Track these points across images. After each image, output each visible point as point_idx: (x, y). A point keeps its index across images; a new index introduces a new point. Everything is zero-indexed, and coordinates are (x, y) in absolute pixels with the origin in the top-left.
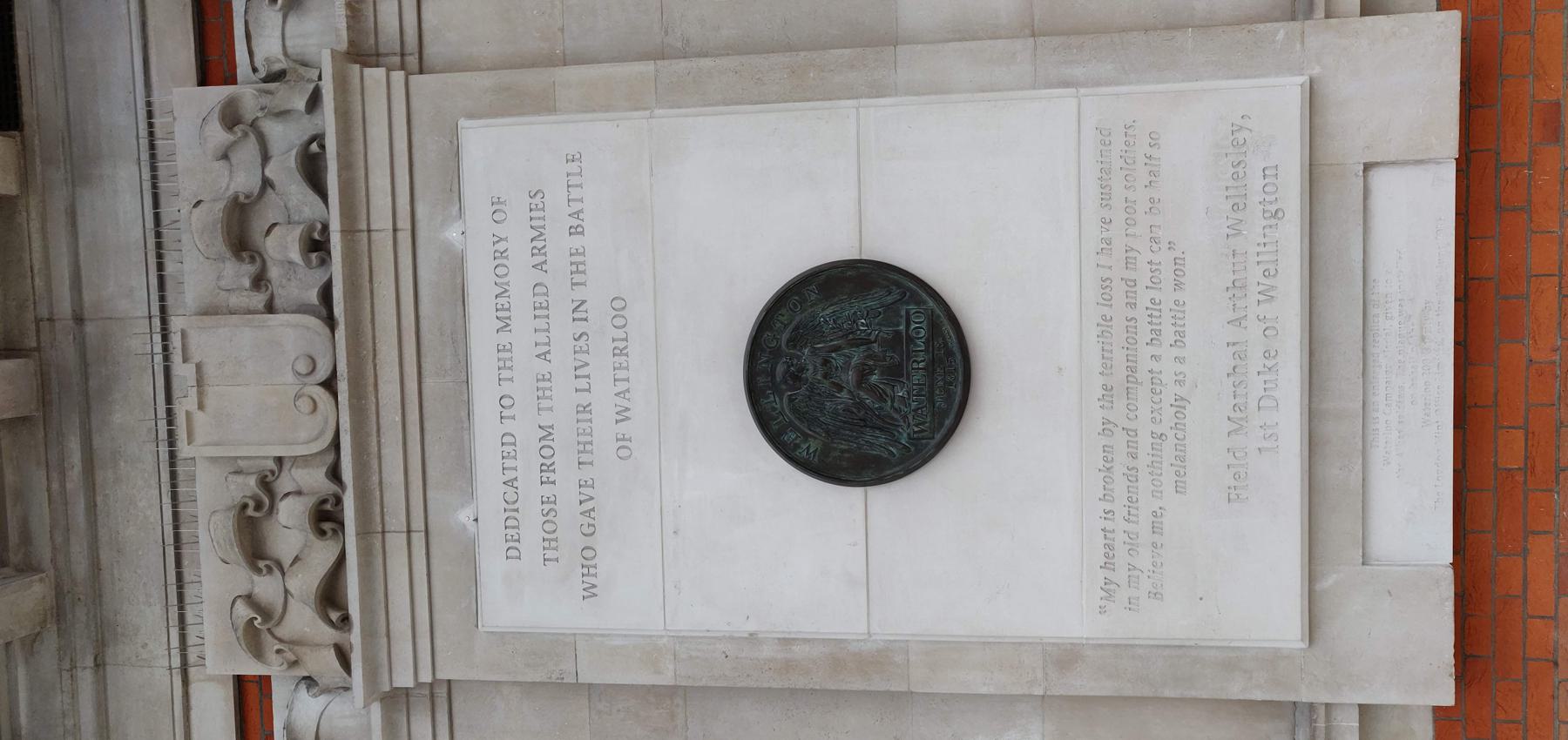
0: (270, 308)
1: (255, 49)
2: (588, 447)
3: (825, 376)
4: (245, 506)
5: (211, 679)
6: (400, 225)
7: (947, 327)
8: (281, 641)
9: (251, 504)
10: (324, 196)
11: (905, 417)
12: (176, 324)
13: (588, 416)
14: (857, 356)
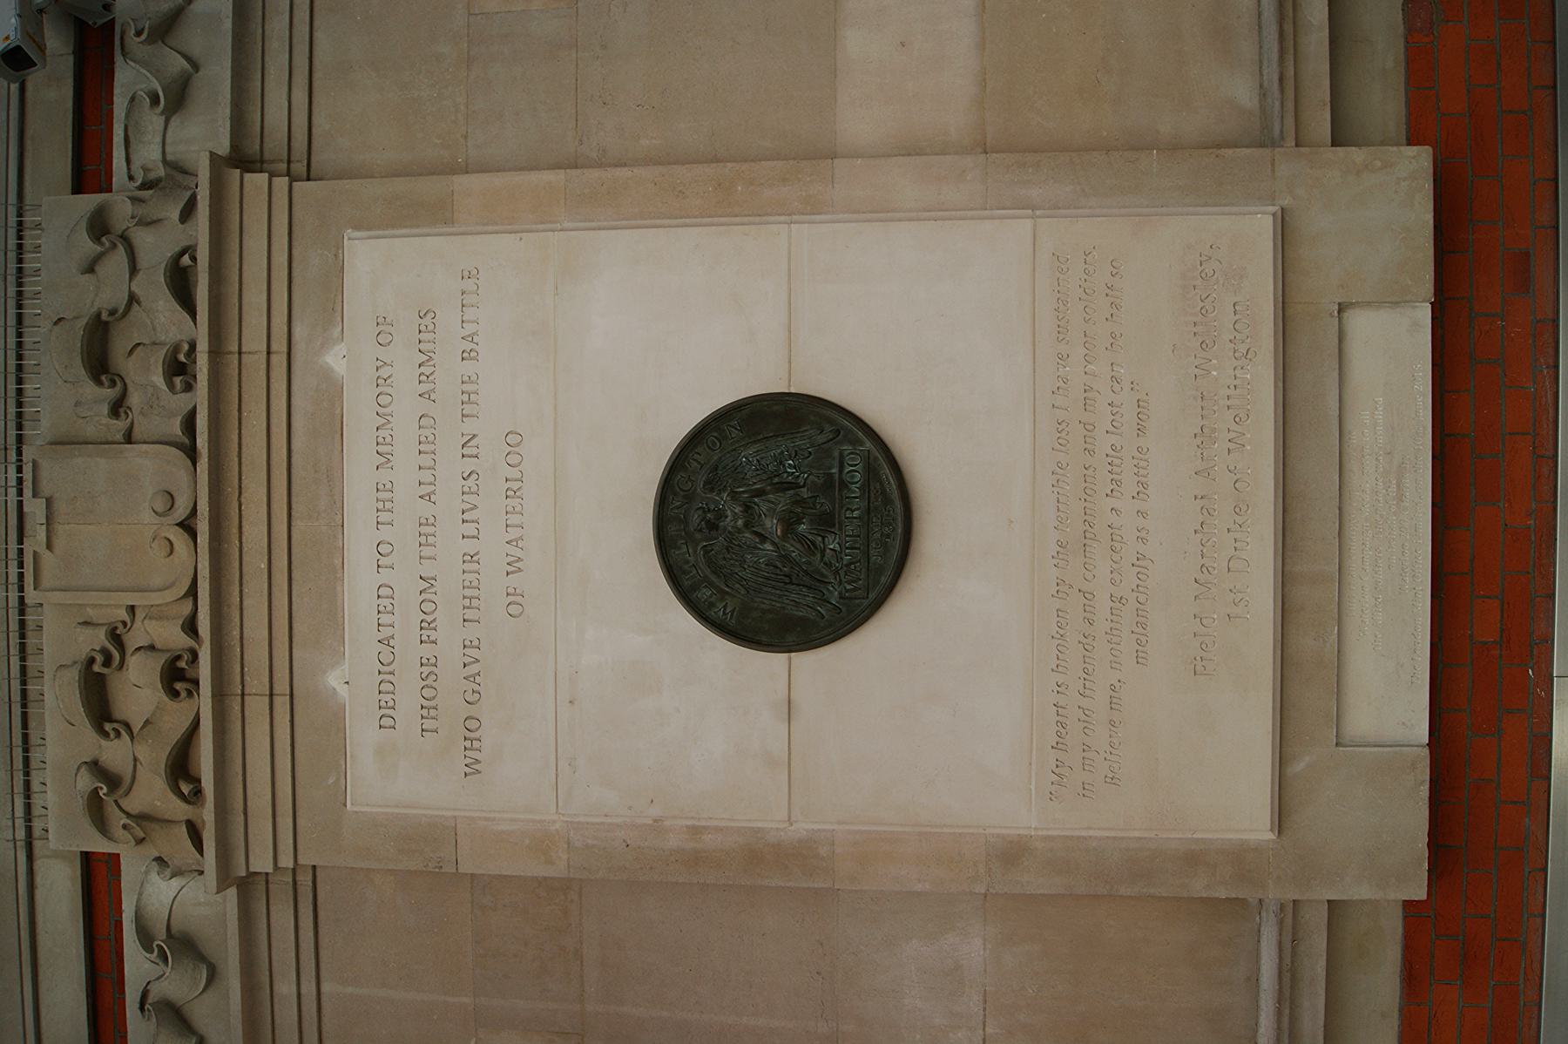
0: (129, 438)
1: (134, 157)
2: (475, 603)
3: (746, 525)
4: (92, 661)
5: (57, 855)
6: (274, 347)
7: (886, 471)
8: (128, 815)
9: (99, 658)
10: (192, 312)
11: (836, 572)
12: (28, 453)
13: (475, 566)
14: (783, 501)
